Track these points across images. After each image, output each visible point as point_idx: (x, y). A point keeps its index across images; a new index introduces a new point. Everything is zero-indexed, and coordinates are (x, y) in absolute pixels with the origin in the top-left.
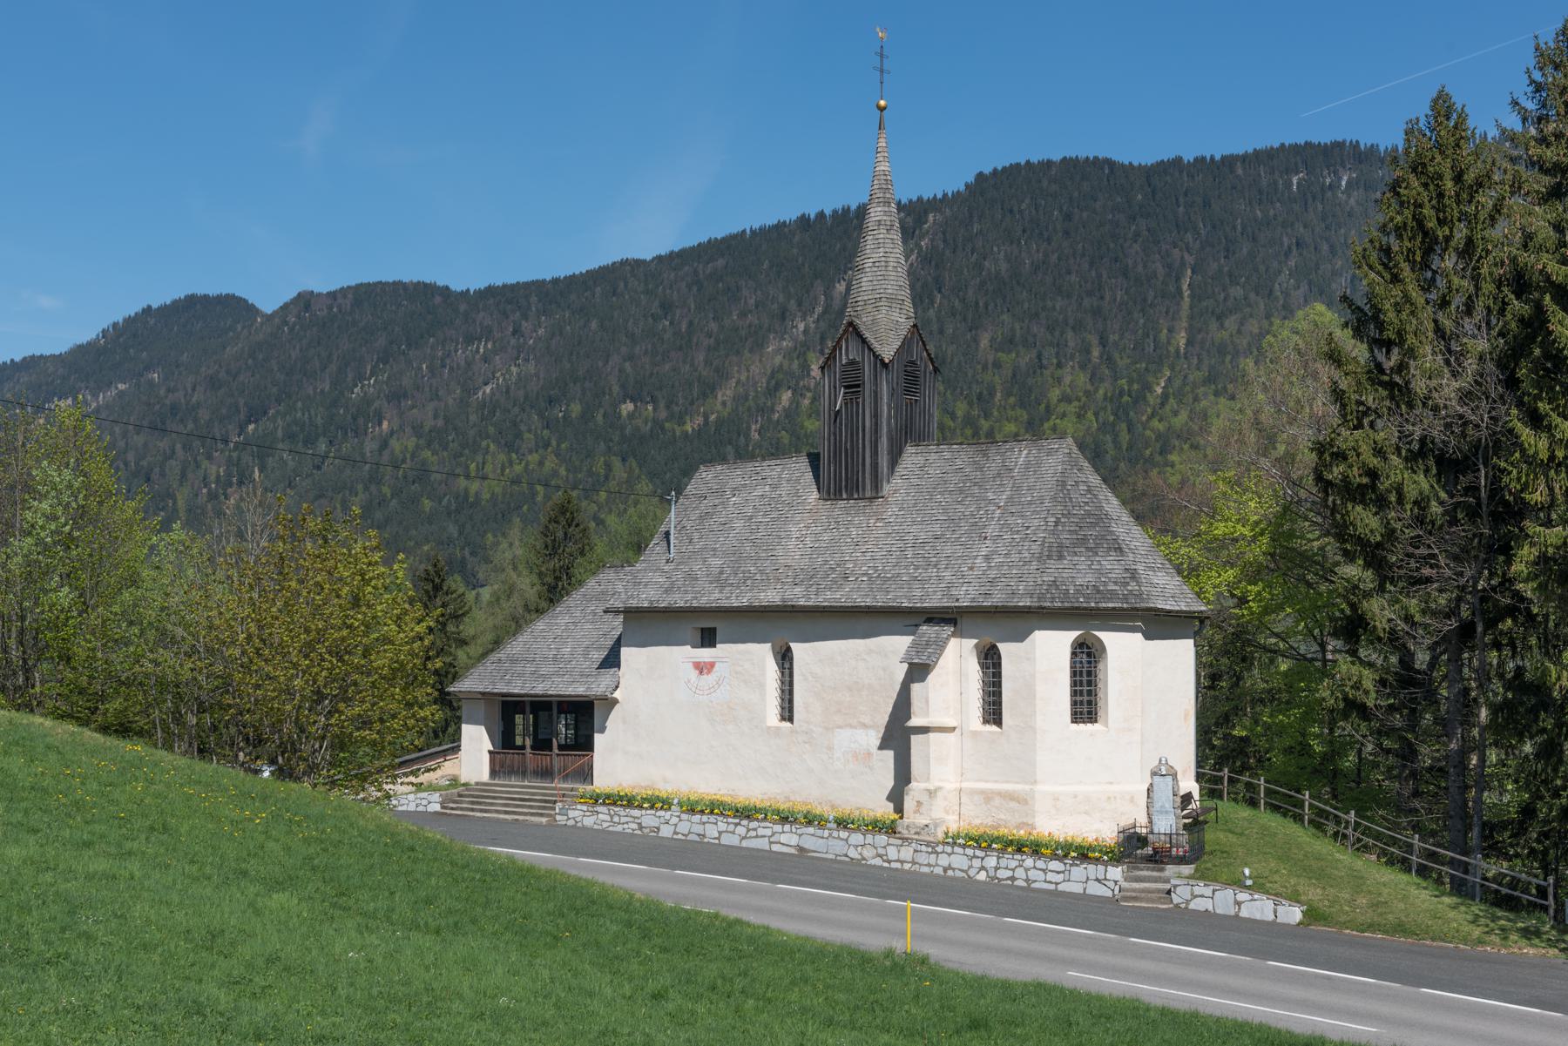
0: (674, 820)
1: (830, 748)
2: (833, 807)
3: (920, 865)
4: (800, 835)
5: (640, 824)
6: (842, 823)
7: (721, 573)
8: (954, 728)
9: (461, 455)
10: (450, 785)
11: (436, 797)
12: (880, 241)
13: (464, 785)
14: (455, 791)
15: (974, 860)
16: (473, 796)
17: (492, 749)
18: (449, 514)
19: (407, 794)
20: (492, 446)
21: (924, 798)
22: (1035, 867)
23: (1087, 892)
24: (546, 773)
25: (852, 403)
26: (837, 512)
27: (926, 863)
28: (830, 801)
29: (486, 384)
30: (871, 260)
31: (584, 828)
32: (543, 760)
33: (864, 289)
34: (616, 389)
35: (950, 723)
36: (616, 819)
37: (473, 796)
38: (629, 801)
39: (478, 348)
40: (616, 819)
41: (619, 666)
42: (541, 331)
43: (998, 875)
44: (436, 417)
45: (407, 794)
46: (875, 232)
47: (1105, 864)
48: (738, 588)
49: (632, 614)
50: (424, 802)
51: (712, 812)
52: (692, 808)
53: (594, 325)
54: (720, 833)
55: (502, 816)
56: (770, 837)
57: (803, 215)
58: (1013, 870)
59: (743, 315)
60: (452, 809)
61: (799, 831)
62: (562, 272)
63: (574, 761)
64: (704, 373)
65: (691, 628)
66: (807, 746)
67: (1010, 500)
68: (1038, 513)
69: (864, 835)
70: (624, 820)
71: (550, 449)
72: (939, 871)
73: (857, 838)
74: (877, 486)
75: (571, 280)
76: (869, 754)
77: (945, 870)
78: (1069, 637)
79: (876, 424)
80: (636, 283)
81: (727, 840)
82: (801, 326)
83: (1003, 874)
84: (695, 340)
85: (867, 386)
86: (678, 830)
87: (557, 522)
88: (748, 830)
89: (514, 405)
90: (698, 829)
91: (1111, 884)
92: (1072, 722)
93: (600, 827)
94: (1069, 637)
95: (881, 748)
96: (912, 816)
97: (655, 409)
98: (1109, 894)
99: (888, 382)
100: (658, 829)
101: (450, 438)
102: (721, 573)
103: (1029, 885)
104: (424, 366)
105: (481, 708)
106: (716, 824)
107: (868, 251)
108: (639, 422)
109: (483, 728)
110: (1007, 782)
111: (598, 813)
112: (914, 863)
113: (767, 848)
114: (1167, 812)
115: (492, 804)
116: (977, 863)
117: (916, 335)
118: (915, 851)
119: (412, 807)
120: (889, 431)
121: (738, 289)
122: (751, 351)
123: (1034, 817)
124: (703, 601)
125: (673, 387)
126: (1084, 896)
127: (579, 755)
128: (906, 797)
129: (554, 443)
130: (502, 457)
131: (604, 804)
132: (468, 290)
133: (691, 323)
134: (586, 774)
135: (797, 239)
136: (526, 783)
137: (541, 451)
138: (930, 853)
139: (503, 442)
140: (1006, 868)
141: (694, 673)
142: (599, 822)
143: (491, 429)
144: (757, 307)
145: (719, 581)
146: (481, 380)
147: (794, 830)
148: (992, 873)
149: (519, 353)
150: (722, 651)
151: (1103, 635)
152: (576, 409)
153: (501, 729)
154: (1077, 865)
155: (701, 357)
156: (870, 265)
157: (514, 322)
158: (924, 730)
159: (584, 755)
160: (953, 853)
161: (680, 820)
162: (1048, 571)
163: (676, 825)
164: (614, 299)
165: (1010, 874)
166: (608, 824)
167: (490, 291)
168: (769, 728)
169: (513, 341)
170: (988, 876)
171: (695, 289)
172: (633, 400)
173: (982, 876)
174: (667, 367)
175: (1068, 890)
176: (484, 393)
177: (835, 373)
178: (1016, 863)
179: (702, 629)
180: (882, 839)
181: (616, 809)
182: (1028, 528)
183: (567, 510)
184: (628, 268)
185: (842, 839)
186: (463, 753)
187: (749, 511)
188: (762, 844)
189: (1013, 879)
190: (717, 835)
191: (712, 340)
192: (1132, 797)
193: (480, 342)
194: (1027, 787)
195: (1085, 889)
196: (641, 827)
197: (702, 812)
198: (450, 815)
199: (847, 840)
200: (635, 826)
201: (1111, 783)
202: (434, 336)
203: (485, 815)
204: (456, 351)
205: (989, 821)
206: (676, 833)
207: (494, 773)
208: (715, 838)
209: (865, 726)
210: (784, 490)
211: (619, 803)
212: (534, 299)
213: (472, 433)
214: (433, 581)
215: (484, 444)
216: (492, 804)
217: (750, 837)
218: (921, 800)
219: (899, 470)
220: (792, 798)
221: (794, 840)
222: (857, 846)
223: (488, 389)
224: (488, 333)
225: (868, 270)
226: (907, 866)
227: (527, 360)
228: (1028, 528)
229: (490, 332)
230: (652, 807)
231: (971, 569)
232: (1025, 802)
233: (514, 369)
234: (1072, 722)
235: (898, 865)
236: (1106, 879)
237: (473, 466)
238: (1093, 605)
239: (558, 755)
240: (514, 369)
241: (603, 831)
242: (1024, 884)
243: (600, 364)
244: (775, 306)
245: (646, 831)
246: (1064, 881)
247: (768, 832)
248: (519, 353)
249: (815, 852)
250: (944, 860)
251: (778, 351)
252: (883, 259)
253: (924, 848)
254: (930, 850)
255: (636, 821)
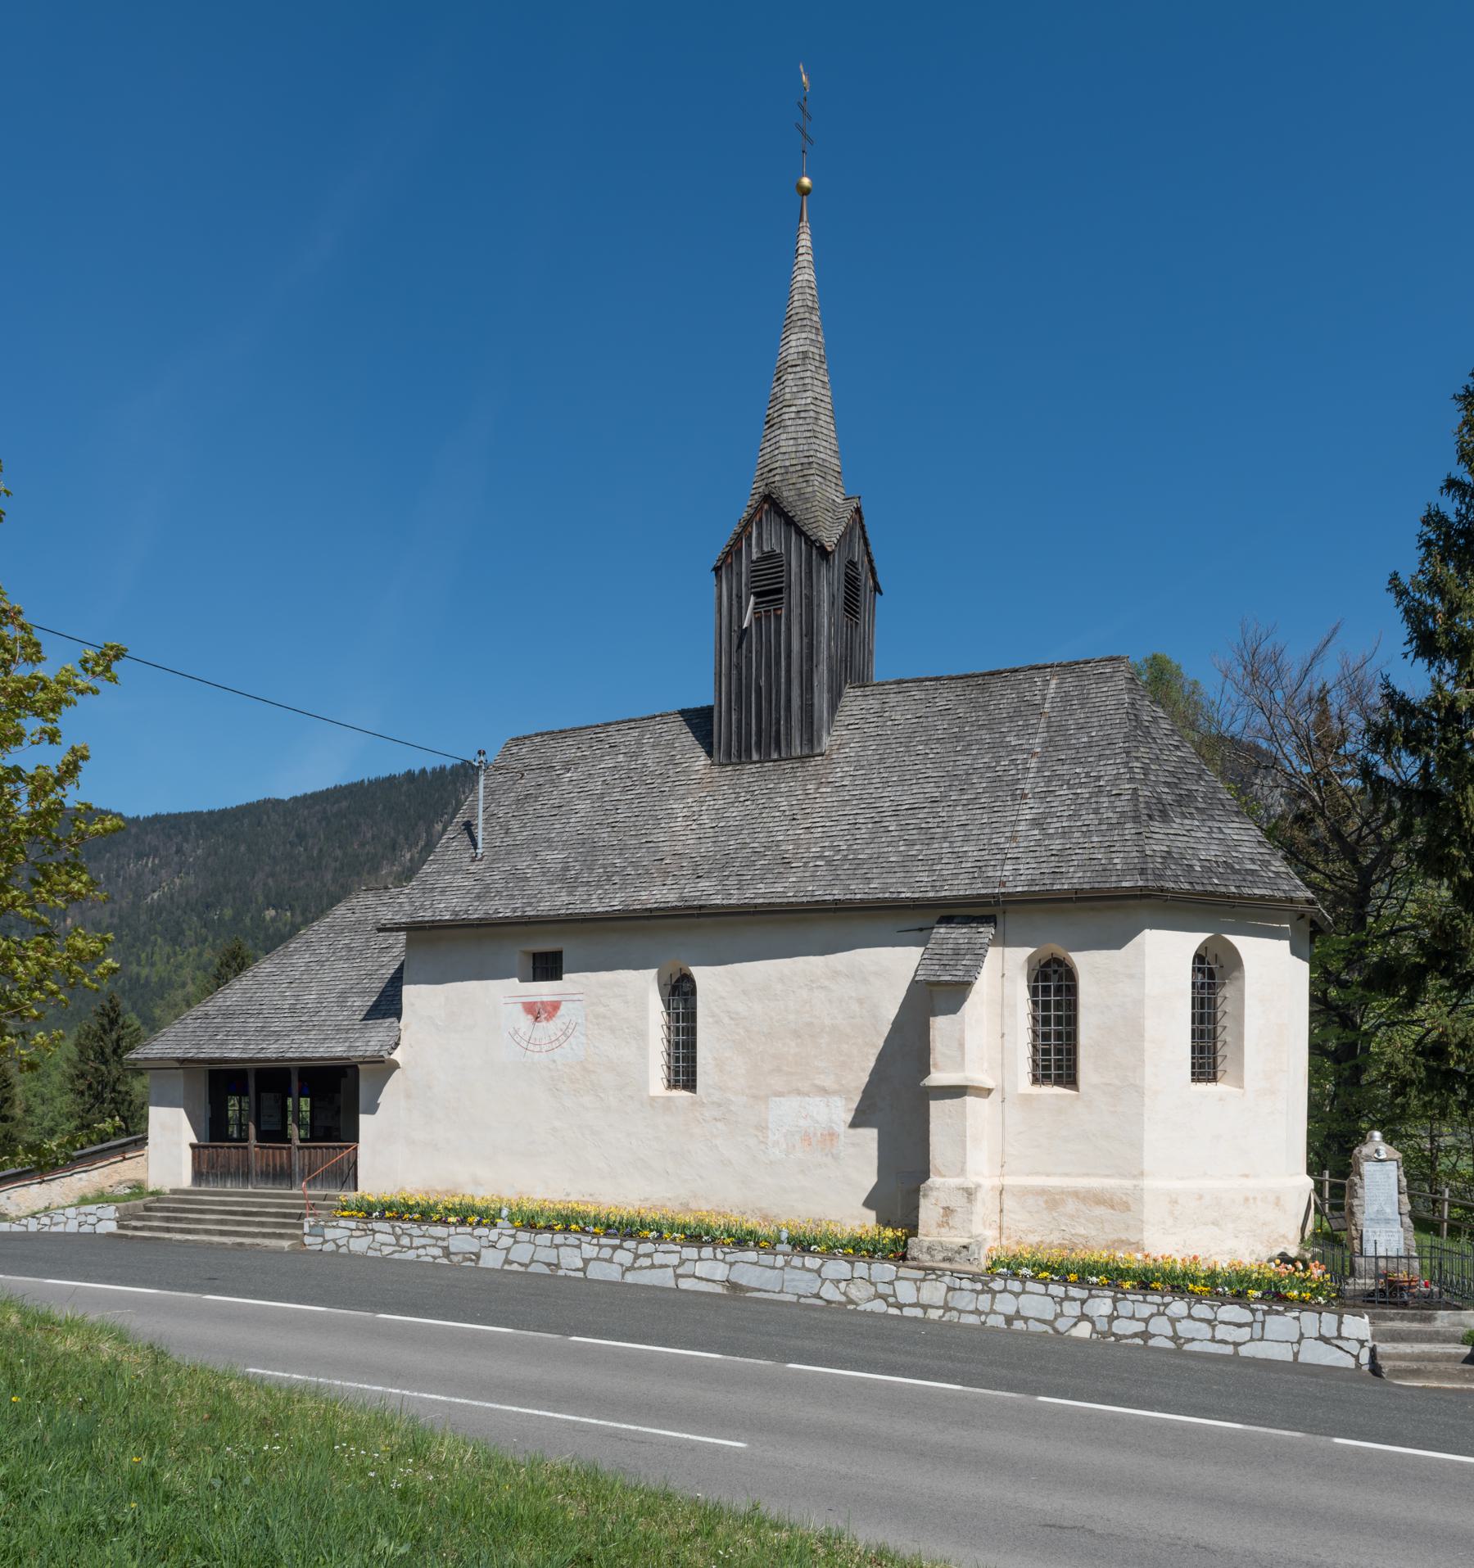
0: (506, 1242)
1: (762, 1127)
2: (765, 1218)
3: (960, 1312)
4: (732, 1264)
5: (445, 1249)
6: (801, 1245)
7: (566, 869)
8: (989, 1091)
9: (134, 946)
10: (131, 1194)
11: (110, 1211)
12: (807, 381)
13: (152, 1193)
14: (140, 1202)
15: (1066, 1304)
16: (168, 1210)
17: (195, 1141)
18: (123, 993)
19: (64, 1208)
20: (159, 940)
21: (957, 1202)
22: (1190, 1316)
23: (1301, 1359)
24: (282, 1175)
25: (768, 618)
26: (746, 779)
27: (971, 1307)
28: (760, 1210)
29: (154, 891)
30: (793, 409)
31: (351, 1255)
32: (277, 1155)
33: (783, 450)
34: (261, 899)
35: (989, 1084)
36: (405, 1241)
37: (168, 1210)
38: (422, 1214)
39: (147, 863)
40: (405, 1241)
41: (398, 1015)
42: (199, 852)
43: (1114, 1330)
44: (112, 915)
45: (64, 1208)
46: (798, 369)
47: (1319, 1310)
48: (599, 887)
49: (421, 932)
50: (92, 1219)
51: (567, 1229)
52: (530, 1223)
53: (243, 848)
54: (586, 1261)
55: (216, 1239)
56: (675, 1267)
57: (409, 771)
58: (1146, 1321)
59: (362, 845)
60: (136, 1228)
61: (729, 1258)
62: (217, 806)
63: (328, 1156)
64: (332, 889)
65: (519, 951)
66: (719, 1125)
67: (1048, 743)
68: (1108, 757)
69: (852, 1263)
70: (417, 1242)
71: (207, 944)
72: (997, 1321)
73: (838, 1268)
74: (811, 737)
75: (224, 813)
76: (832, 1135)
77: (1009, 1320)
78: (1192, 941)
79: (811, 645)
80: (277, 817)
81: (596, 1272)
82: (408, 856)
83: (1122, 1327)
84: (324, 863)
85: (795, 588)
86: (511, 1257)
87: (228, 966)
88: (637, 1257)
89: (177, 909)
90: (550, 1255)
91: (1353, 1347)
92: (1193, 1080)
93: (378, 1254)
94: (1192, 941)
95: (855, 1124)
96: (934, 1231)
97: (292, 915)
98: (1350, 1363)
99: (829, 584)
100: (478, 1256)
101: (124, 933)
102: (566, 869)
103: (1180, 1347)
104: (102, 876)
105: (178, 1084)
106: (579, 1247)
107: (788, 396)
108: (280, 925)
109: (182, 1111)
110: (1087, 1175)
111: (374, 1232)
112: (947, 1308)
113: (672, 1284)
114: (1387, 1221)
115: (199, 1221)
116: (1072, 1309)
117: (858, 531)
118: (950, 1289)
119: (72, 1227)
120: (830, 657)
121: (359, 825)
122: (369, 873)
123: (1142, 1230)
124: (544, 907)
125: (307, 898)
126: (1295, 1366)
127: (334, 1148)
128: (922, 1202)
129: (210, 939)
130: (168, 949)
131: (382, 1218)
132: (138, 817)
133: (321, 850)
134: (347, 1175)
135: (405, 788)
136: (250, 1190)
137: (199, 945)
138: (978, 1293)
139: (168, 937)
140: (1133, 1317)
141: (525, 1021)
142: (377, 1246)
143: (159, 927)
144: (373, 839)
145: (564, 878)
146: (150, 888)
147: (720, 1256)
148: (1102, 1325)
149: (181, 867)
150: (572, 982)
151: (1237, 941)
152: (228, 913)
153: (209, 1115)
154: (1278, 1313)
155: (329, 876)
156: (793, 415)
157: (177, 843)
158: (957, 1092)
159: (341, 1148)
160: (1024, 1292)
161: (516, 1242)
162: (1155, 836)
163: (508, 1249)
164: (259, 828)
165: (1139, 1327)
166: (392, 1249)
167: (157, 819)
168: (653, 1099)
169: (176, 859)
170: (1094, 1330)
171: (324, 823)
172: (274, 907)
173: (1083, 1330)
174: (302, 883)
175: (656, 1283)
176: (152, 899)
177: (739, 574)
178: (1154, 1309)
179: (534, 955)
180: (885, 1270)
181: (405, 1226)
182: (1099, 778)
183: (238, 955)
184: (270, 805)
185: (809, 1270)
186: (151, 1149)
187: (597, 786)
188: (665, 1279)
189: (1146, 1335)
190: (580, 1264)
191: (338, 863)
192: (1278, 1198)
193: (148, 858)
194: (1128, 1183)
195: (1296, 1355)
196: (447, 1252)
197: (549, 1228)
198: (133, 1237)
199: (818, 1272)
200: (437, 1252)
201: (1246, 1176)
202: (109, 852)
203: (190, 1237)
204: (129, 865)
205: (1055, 1238)
206: (507, 1261)
207: (198, 1175)
208: (578, 1270)
209: (824, 1091)
210: (650, 758)
211: (407, 1216)
212: (193, 826)
213: (142, 930)
214: (108, 1016)
215: (153, 938)
216: (199, 1221)
217: (641, 1268)
218: (952, 1205)
219: (842, 717)
220: (693, 1206)
221: (720, 1272)
222: (839, 1281)
223: (155, 896)
224: (155, 852)
225: (789, 423)
226: (934, 1314)
227: (187, 874)
228: (1099, 778)
229: (157, 850)
230: (463, 1222)
231: (1013, 838)
232: (1127, 1207)
233: (177, 881)
234: (1193, 1080)
235: (918, 1312)
236: (1340, 1337)
237: (143, 956)
238: (1233, 889)
239: (299, 1148)
240: (177, 881)
241: (385, 1259)
242: (1170, 1345)
243: (248, 879)
244: (388, 839)
245: (455, 1259)
246: (1252, 1339)
247: (673, 1259)
248: (181, 867)
249: (759, 1290)
250: (1006, 1305)
251: (390, 874)
252: (812, 407)
253: (966, 1284)
254: (979, 1286)
255: (440, 1243)
